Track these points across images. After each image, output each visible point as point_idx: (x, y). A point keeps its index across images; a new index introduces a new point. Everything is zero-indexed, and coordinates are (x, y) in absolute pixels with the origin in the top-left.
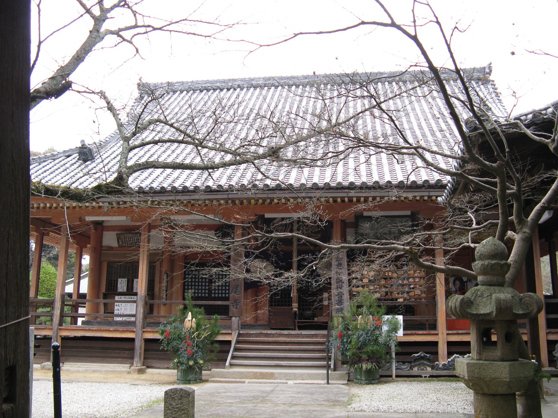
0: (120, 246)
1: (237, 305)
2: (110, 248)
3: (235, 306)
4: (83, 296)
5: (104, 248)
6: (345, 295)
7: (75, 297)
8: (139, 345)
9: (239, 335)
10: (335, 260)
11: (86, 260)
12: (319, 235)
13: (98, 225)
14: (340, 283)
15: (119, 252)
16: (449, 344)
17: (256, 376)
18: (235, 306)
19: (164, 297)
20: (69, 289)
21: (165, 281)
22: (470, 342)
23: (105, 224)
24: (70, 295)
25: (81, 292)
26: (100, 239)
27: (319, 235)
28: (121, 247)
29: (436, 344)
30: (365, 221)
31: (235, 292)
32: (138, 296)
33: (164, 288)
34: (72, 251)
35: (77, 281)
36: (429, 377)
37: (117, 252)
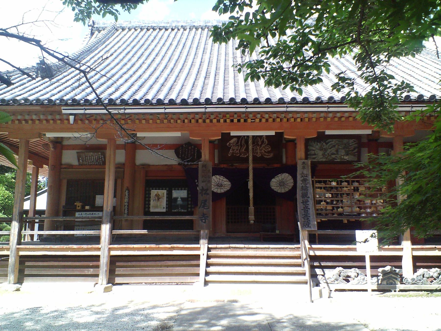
0: (80, 165)
1: (205, 219)
2: (70, 166)
3: (204, 221)
4: (41, 212)
5: (64, 166)
6: (311, 210)
7: (31, 215)
8: (104, 261)
9: (209, 249)
10: (301, 176)
11: (43, 179)
12: (272, 154)
13: (58, 143)
14: (306, 198)
15: (80, 170)
16: (416, 259)
17: (35, 270)
18: (204, 221)
19: (126, 212)
20: (27, 206)
21: (127, 197)
22: (199, 255)
23: (65, 143)
24: (26, 212)
25: (36, 209)
26: (59, 157)
27: (272, 154)
28: (82, 165)
29: (399, 258)
30: (314, 142)
31: (204, 207)
32: (104, 212)
33: (126, 204)
34: (30, 169)
35: (33, 198)
36: (399, 291)
37: (78, 170)
